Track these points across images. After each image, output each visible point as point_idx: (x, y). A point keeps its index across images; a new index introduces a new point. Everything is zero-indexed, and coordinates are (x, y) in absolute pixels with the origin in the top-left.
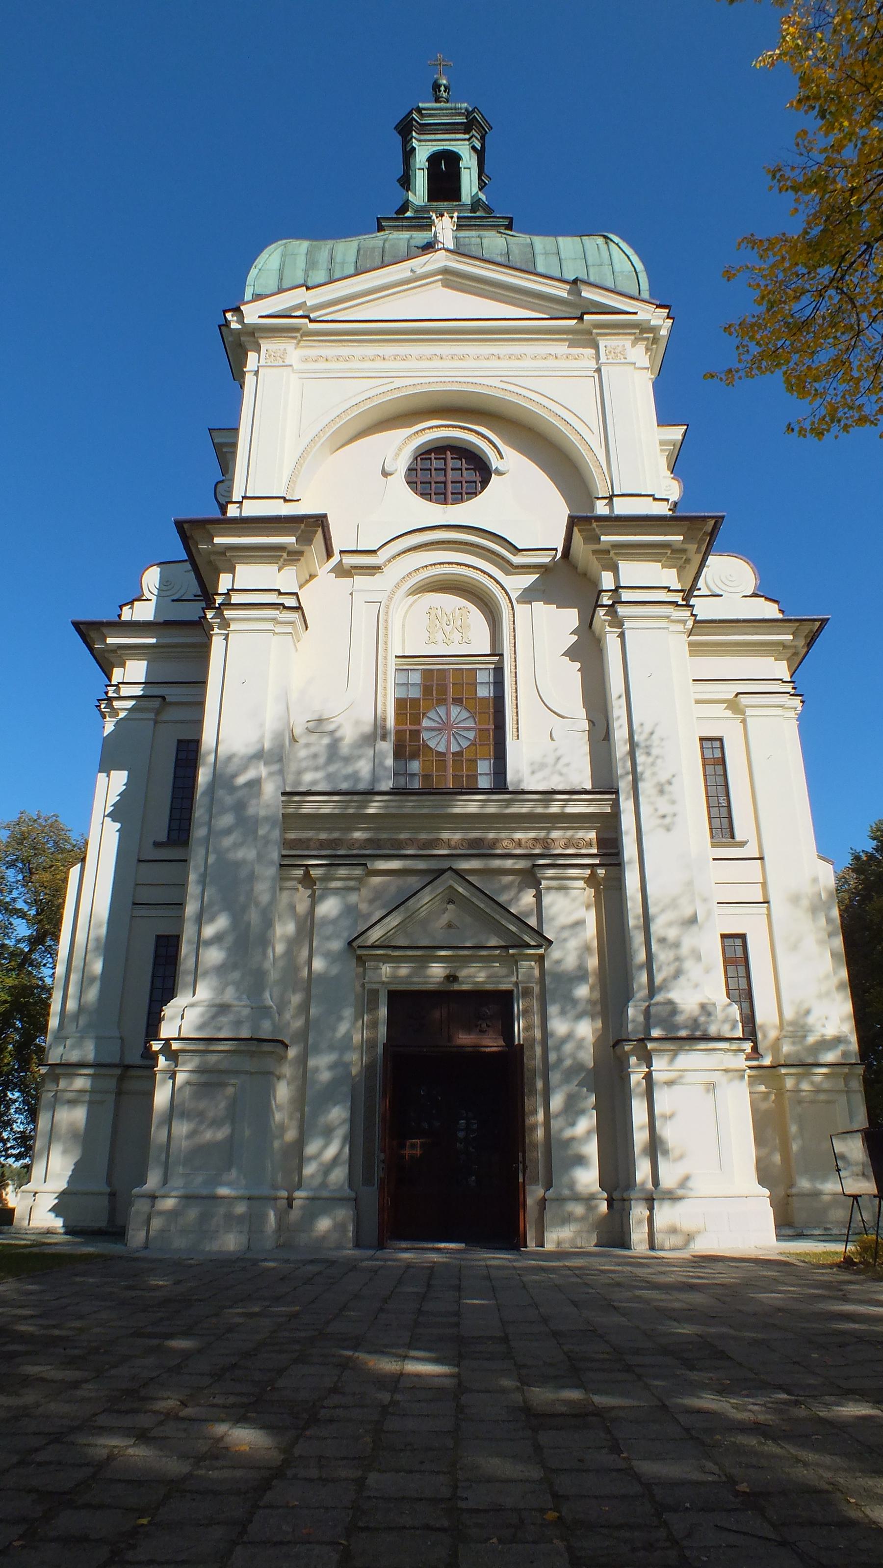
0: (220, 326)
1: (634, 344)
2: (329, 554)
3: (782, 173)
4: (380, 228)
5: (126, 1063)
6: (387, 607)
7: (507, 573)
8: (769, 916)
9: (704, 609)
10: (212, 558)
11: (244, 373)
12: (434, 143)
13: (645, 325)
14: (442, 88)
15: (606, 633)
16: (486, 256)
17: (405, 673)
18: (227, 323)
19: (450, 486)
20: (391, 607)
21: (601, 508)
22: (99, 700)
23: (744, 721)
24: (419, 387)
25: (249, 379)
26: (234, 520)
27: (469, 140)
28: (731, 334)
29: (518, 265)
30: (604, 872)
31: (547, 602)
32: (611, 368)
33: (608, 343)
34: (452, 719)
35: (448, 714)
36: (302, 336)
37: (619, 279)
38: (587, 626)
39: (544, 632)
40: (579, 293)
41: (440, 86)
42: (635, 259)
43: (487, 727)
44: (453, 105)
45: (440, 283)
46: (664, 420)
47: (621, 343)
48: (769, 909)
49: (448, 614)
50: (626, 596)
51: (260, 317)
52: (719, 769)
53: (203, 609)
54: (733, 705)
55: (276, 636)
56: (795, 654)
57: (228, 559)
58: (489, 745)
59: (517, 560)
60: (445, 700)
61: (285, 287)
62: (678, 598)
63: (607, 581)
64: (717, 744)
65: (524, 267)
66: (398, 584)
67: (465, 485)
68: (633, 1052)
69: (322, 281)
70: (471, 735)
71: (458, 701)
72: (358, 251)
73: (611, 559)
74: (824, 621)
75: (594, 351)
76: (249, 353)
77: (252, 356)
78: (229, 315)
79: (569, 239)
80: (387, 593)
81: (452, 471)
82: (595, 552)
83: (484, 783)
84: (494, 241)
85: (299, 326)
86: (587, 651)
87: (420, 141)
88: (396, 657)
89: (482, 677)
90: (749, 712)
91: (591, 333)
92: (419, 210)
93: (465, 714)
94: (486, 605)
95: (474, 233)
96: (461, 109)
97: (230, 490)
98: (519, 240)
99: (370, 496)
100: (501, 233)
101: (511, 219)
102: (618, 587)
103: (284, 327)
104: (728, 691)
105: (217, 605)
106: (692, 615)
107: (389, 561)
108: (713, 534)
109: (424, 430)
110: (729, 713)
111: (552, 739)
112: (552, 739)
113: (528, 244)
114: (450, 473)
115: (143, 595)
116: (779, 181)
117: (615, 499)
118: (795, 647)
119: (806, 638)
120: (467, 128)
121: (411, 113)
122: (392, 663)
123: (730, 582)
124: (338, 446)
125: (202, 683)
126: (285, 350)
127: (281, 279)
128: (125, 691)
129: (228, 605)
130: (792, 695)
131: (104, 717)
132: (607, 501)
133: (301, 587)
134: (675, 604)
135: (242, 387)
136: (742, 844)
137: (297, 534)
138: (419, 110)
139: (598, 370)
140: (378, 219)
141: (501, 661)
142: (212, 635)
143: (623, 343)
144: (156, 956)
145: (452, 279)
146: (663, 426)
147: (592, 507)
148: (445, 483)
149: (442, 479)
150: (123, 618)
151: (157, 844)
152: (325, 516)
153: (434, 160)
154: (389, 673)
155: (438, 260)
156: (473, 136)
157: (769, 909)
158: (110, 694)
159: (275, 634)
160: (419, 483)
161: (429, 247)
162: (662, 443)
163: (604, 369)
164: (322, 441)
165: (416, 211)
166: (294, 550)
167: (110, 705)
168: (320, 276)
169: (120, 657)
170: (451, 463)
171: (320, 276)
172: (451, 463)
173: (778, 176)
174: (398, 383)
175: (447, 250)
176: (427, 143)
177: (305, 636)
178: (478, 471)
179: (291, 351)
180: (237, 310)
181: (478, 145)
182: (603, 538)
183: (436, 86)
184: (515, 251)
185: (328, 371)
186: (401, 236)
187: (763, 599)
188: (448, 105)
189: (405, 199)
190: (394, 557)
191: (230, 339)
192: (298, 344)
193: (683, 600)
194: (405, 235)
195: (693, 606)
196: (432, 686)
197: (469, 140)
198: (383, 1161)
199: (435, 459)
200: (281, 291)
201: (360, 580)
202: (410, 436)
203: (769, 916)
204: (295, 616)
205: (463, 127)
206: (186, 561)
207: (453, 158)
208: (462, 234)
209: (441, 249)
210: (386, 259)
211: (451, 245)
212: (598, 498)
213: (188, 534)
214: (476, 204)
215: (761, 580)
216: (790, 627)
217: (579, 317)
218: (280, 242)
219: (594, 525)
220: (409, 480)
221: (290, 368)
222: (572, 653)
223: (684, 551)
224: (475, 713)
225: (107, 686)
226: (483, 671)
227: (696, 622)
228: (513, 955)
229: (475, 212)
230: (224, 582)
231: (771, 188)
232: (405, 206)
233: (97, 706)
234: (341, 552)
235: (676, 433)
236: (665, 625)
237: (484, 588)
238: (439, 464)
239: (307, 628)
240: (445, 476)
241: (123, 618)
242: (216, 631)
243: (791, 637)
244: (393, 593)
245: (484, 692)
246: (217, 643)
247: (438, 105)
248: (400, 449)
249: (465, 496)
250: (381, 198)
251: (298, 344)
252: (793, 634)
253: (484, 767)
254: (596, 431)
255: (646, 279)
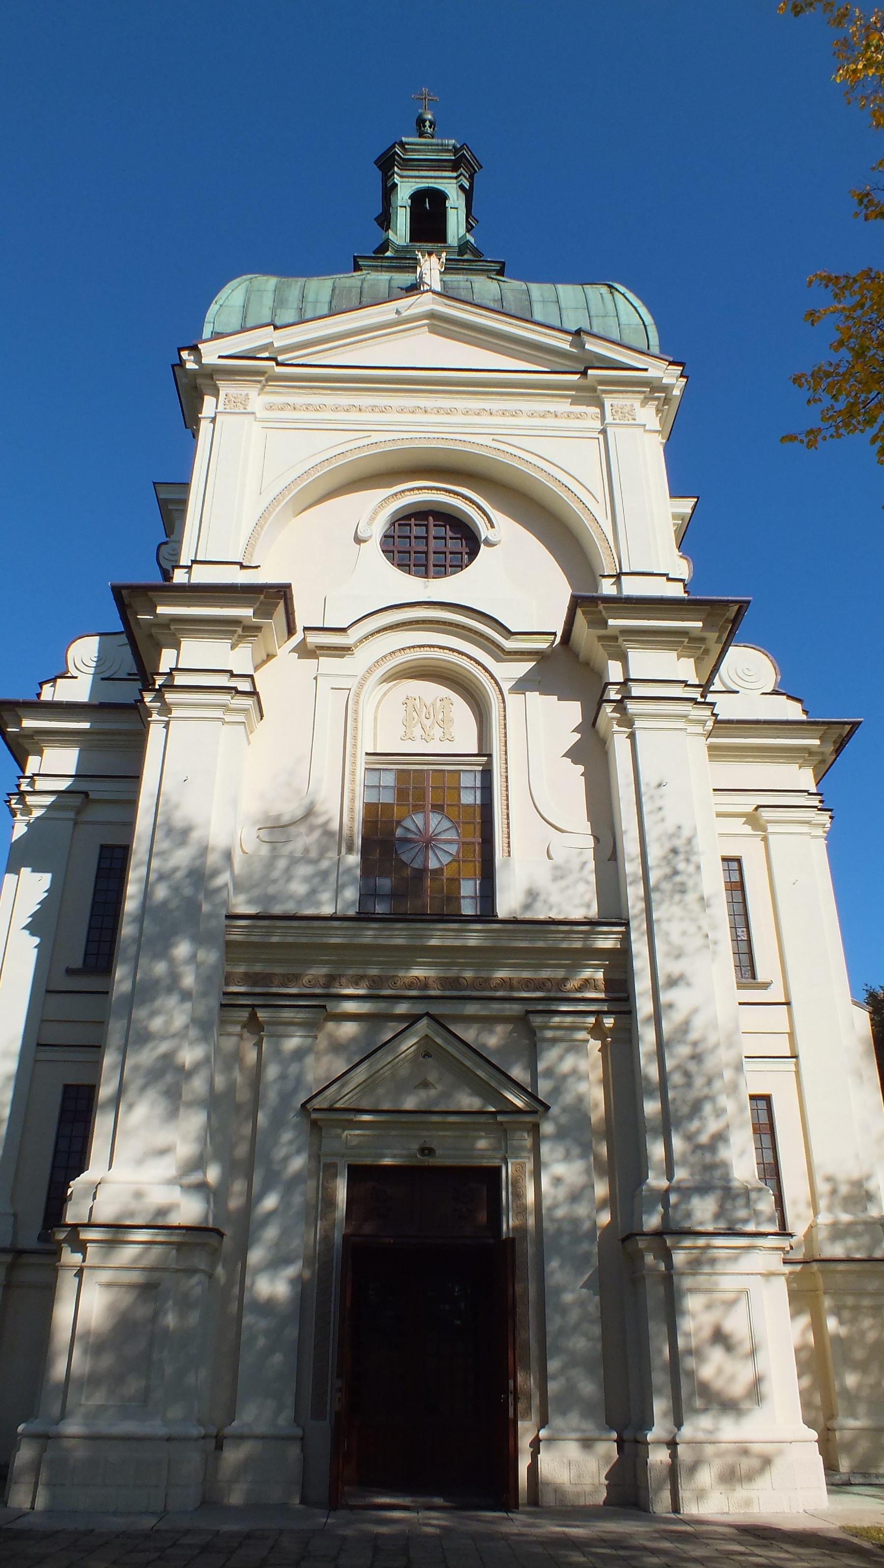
0: (173, 366)
1: (644, 403)
2: (291, 631)
3: (870, 197)
4: (357, 268)
5: (20, 1246)
6: (358, 695)
7: (498, 660)
8: (798, 1073)
9: (728, 708)
10: (154, 631)
11: (199, 419)
12: (418, 180)
13: (655, 384)
14: (427, 124)
15: (613, 733)
16: (476, 301)
17: (376, 773)
18: (182, 363)
19: (432, 556)
20: (362, 697)
21: (608, 588)
22: (9, 794)
23: (765, 839)
24: (399, 442)
25: (205, 427)
26: (181, 588)
27: (456, 178)
28: (800, 386)
29: (513, 312)
30: (612, 1020)
31: (544, 692)
32: (619, 430)
33: (615, 402)
34: (431, 830)
35: (426, 823)
36: (267, 380)
37: (626, 331)
38: (590, 725)
39: (540, 729)
40: (583, 346)
41: (424, 121)
42: (643, 311)
43: (472, 840)
44: (440, 141)
45: (426, 329)
46: (676, 493)
47: (629, 402)
48: (797, 1065)
49: (428, 705)
50: (637, 690)
51: (220, 357)
52: (738, 894)
53: (141, 691)
54: (753, 819)
55: (226, 726)
56: (823, 761)
57: (172, 632)
58: (474, 861)
59: (509, 644)
60: (424, 806)
61: (248, 325)
62: (696, 694)
63: (614, 671)
64: (734, 865)
65: (519, 315)
66: (370, 669)
67: (449, 556)
68: (649, 1249)
69: (291, 321)
70: (453, 849)
71: (438, 808)
72: (333, 290)
73: (619, 646)
74: (855, 725)
75: (598, 410)
76: (206, 397)
77: (209, 401)
78: (185, 354)
79: (569, 287)
80: (358, 679)
81: (431, 540)
82: (601, 638)
83: (468, 908)
84: (485, 287)
85: (265, 369)
86: (591, 751)
87: (401, 177)
88: (367, 754)
89: (466, 780)
90: (771, 828)
91: (595, 390)
92: (399, 249)
93: (446, 824)
94: (472, 696)
95: (460, 277)
96: (448, 145)
97: (177, 554)
98: (512, 286)
99: (340, 566)
100: (491, 278)
101: (503, 263)
102: (627, 680)
103: (250, 369)
104: (516, 1009)
105: (157, 687)
106: (713, 714)
107: (361, 641)
108: (736, 621)
109: (403, 491)
110: (748, 829)
111: (549, 857)
112: (549, 857)
113: (523, 290)
114: (433, 543)
115: (68, 671)
116: (866, 207)
117: (623, 577)
118: (822, 753)
119: (835, 741)
120: (455, 166)
121: (393, 146)
122: (362, 762)
123: (750, 677)
124: (304, 507)
125: (136, 778)
126: (247, 395)
127: (244, 317)
128: (41, 784)
129: (170, 686)
130: (819, 810)
131: (14, 815)
132: (614, 580)
133: (256, 668)
134: (693, 700)
135: (195, 435)
136: (765, 986)
137: (256, 606)
138: (402, 145)
139: (604, 432)
140: (354, 257)
141: (490, 763)
142: (149, 723)
143: (630, 402)
144: (63, 1111)
145: (439, 324)
146: (676, 497)
147: (596, 586)
148: (426, 553)
149: (424, 549)
150: (43, 698)
151: (70, 972)
152: (288, 586)
153: (417, 197)
154: (358, 773)
155: (424, 303)
156: (461, 174)
157: (797, 1065)
158: (24, 788)
159: (224, 723)
160: (396, 552)
161: (413, 289)
162: (675, 516)
163: (610, 431)
164: (286, 501)
165: (396, 251)
166: (250, 624)
167: (21, 801)
168: (289, 315)
169: (37, 743)
170: (433, 531)
171: (289, 315)
172: (433, 531)
173: (865, 201)
174: (376, 437)
175: (434, 292)
176: (410, 180)
177: (261, 727)
178: (467, 541)
179: (256, 398)
180: (194, 349)
181: (467, 185)
182: (611, 622)
183: (421, 121)
184: (509, 296)
185: (295, 421)
186: (380, 277)
187: (785, 697)
188: (434, 141)
189: (384, 237)
190: (366, 638)
191: (185, 380)
192: (262, 389)
193: (702, 696)
194: (385, 276)
195: (713, 704)
196: (408, 789)
197: (456, 178)
198: (340, 1390)
199: (416, 525)
200: (244, 330)
201: (326, 663)
202: (388, 498)
203: (798, 1073)
204: (249, 702)
205: (450, 164)
206: (121, 633)
207: (439, 197)
208: (447, 278)
209: (427, 291)
210: (364, 299)
211: (438, 287)
212: (604, 576)
213: (126, 602)
214: (464, 247)
215: (781, 675)
216: (818, 730)
217: (583, 373)
218: (244, 277)
219: (601, 606)
220: (385, 549)
221: (252, 417)
222: (574, 754)
223: (702, 640)
224: (458, 823)
225: (19, 778)
226: (467, 774)
227: (717, 722)
228: (501, 1123)
229: (462, 256)
230: (167, 659)
231: (857, 214)
232: (385, 245)
233: (6, 802)
234: (306, 629)
235: (686, 506)
236: (681, 725)
237: (465, 673)
238: (421, 531)
239: (262, 717)
240: (427, 545)
241: (43, 698)
242: (155, 717)
243: (818, 742)
244: (364, 679)
245: (469, 798)
246: (155, 732)
247: (423, 140)
248: (375, 513)
249: (449, 569)
250: (361, 236)
251: (262, 389)
252: (820, 738)
253: (468, 888)
254: (600, 498)
255: (656, 334)
